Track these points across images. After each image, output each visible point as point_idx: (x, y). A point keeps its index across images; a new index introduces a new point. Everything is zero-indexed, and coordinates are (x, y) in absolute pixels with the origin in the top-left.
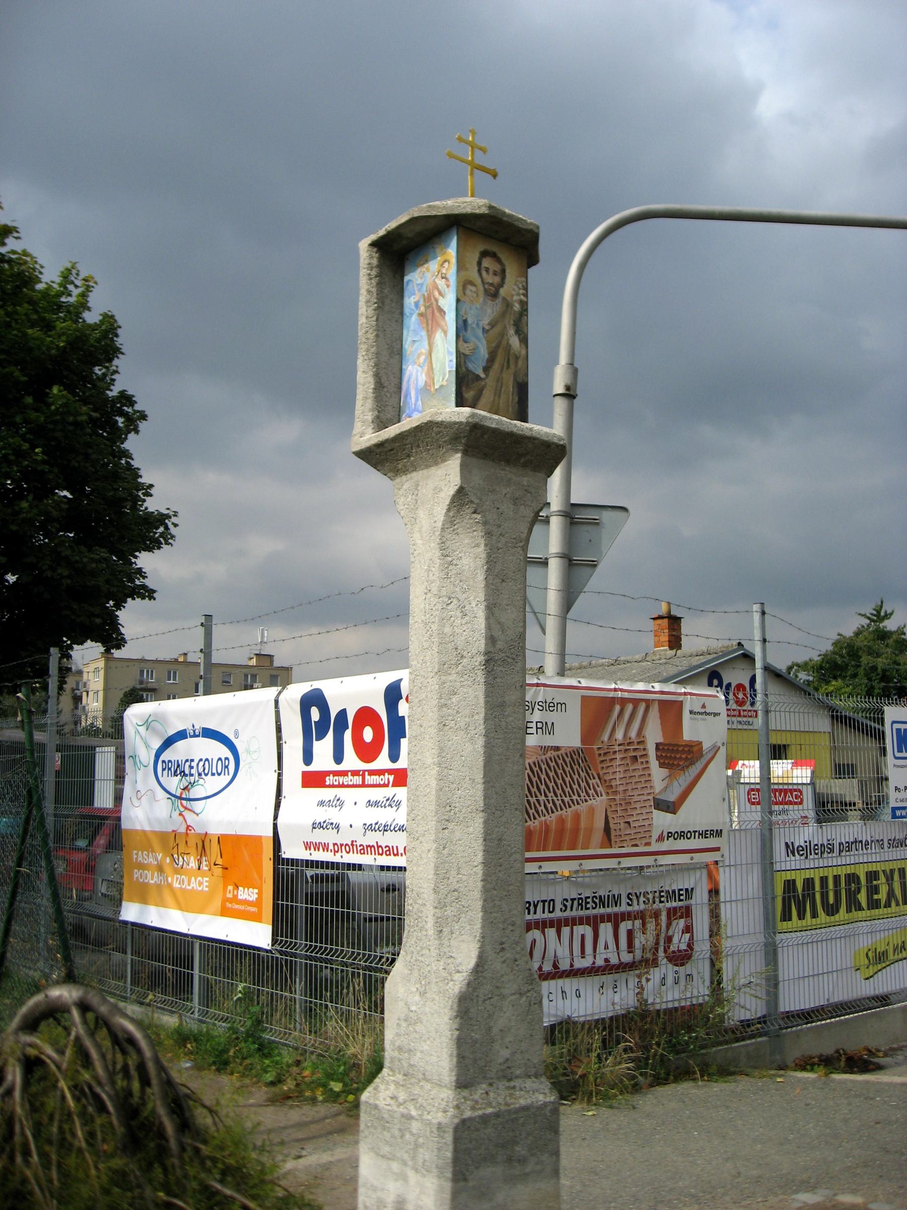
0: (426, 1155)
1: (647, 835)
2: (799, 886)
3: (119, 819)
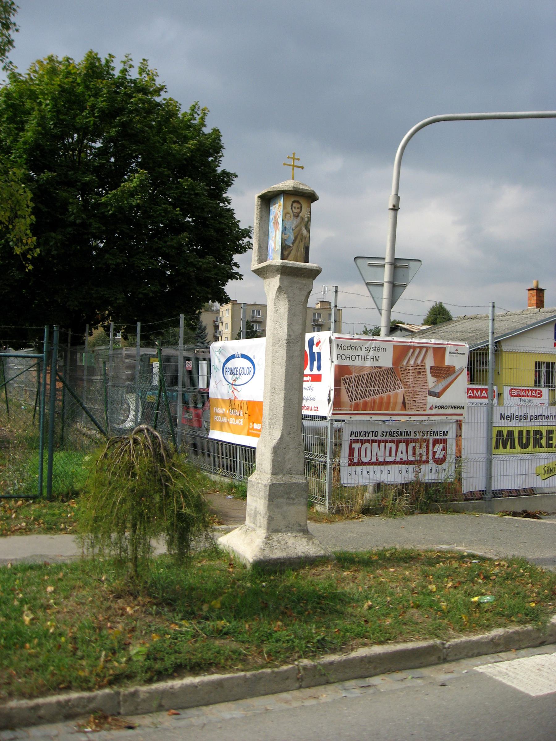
0: (262, 494)
1: (424, 406)
2: (505, 434)
3: (208, 393)
